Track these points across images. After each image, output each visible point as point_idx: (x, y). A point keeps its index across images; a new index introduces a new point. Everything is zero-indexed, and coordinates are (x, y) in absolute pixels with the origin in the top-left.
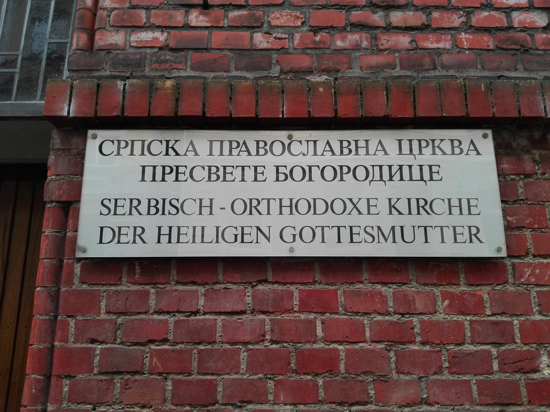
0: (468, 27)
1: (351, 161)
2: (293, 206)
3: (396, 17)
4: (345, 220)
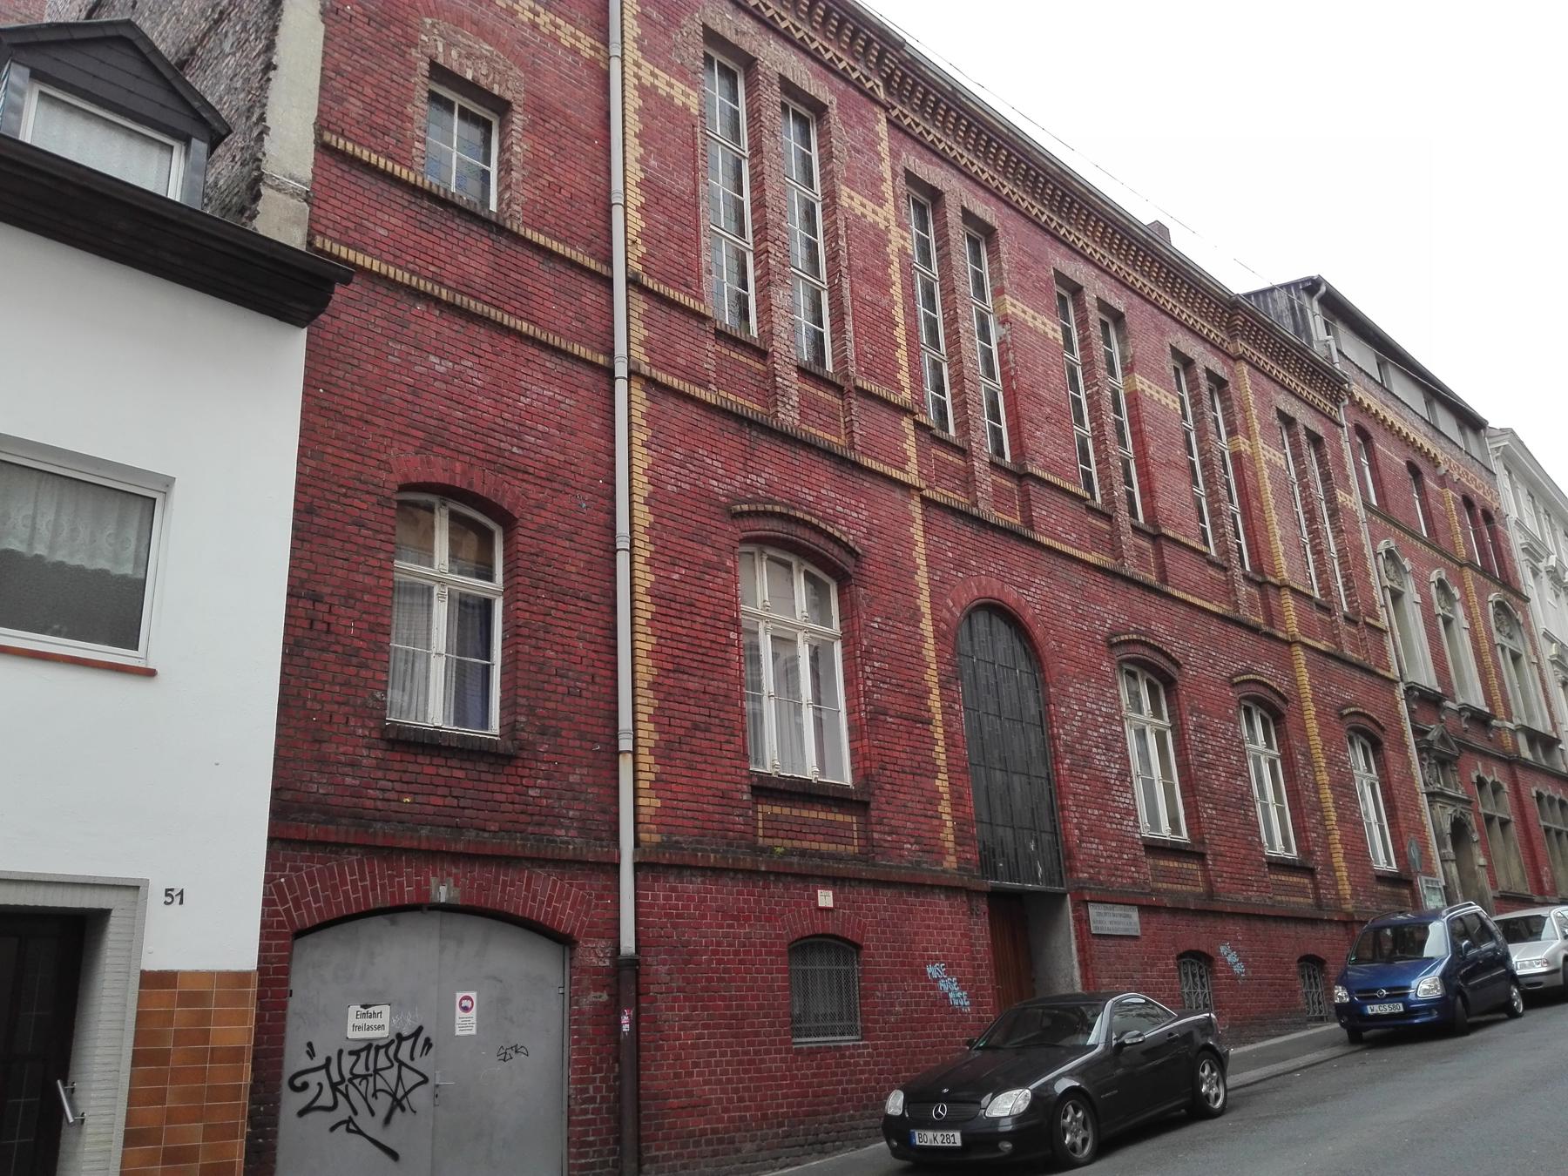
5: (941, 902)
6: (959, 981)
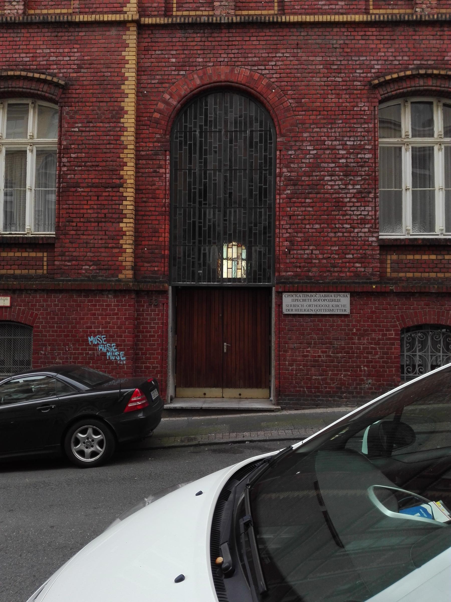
0: (349, 271)
1: (326, 298)
2: (316, 306)
3: (336, 269)
4: (325, 308)
5: (111, 299)
6: (117, 346)
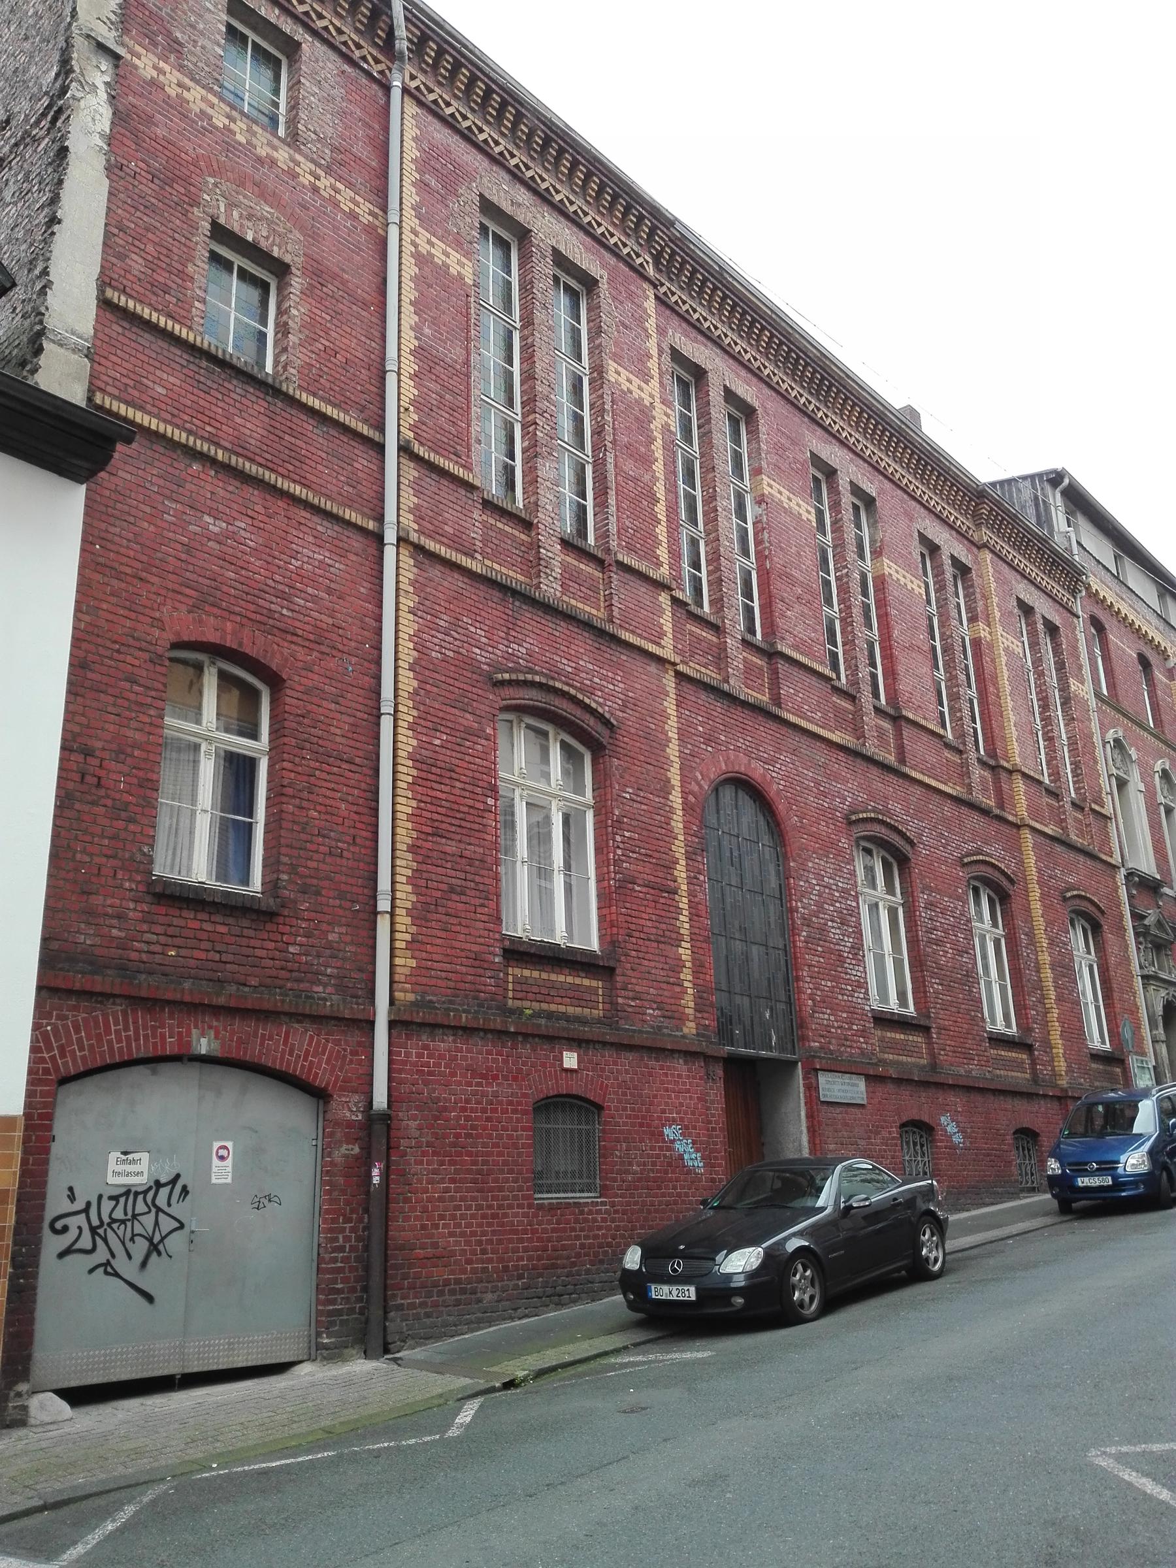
5: (680, 1066)
6: (694, 1143)
